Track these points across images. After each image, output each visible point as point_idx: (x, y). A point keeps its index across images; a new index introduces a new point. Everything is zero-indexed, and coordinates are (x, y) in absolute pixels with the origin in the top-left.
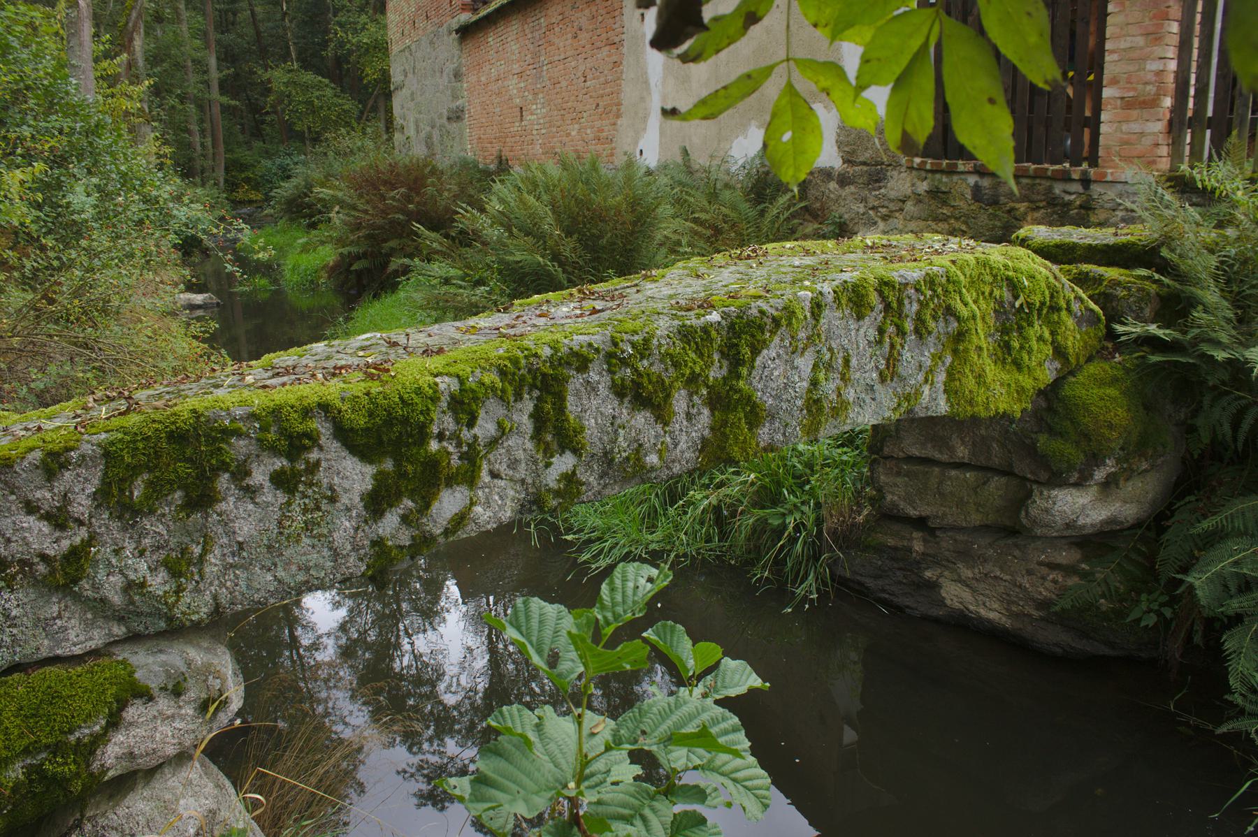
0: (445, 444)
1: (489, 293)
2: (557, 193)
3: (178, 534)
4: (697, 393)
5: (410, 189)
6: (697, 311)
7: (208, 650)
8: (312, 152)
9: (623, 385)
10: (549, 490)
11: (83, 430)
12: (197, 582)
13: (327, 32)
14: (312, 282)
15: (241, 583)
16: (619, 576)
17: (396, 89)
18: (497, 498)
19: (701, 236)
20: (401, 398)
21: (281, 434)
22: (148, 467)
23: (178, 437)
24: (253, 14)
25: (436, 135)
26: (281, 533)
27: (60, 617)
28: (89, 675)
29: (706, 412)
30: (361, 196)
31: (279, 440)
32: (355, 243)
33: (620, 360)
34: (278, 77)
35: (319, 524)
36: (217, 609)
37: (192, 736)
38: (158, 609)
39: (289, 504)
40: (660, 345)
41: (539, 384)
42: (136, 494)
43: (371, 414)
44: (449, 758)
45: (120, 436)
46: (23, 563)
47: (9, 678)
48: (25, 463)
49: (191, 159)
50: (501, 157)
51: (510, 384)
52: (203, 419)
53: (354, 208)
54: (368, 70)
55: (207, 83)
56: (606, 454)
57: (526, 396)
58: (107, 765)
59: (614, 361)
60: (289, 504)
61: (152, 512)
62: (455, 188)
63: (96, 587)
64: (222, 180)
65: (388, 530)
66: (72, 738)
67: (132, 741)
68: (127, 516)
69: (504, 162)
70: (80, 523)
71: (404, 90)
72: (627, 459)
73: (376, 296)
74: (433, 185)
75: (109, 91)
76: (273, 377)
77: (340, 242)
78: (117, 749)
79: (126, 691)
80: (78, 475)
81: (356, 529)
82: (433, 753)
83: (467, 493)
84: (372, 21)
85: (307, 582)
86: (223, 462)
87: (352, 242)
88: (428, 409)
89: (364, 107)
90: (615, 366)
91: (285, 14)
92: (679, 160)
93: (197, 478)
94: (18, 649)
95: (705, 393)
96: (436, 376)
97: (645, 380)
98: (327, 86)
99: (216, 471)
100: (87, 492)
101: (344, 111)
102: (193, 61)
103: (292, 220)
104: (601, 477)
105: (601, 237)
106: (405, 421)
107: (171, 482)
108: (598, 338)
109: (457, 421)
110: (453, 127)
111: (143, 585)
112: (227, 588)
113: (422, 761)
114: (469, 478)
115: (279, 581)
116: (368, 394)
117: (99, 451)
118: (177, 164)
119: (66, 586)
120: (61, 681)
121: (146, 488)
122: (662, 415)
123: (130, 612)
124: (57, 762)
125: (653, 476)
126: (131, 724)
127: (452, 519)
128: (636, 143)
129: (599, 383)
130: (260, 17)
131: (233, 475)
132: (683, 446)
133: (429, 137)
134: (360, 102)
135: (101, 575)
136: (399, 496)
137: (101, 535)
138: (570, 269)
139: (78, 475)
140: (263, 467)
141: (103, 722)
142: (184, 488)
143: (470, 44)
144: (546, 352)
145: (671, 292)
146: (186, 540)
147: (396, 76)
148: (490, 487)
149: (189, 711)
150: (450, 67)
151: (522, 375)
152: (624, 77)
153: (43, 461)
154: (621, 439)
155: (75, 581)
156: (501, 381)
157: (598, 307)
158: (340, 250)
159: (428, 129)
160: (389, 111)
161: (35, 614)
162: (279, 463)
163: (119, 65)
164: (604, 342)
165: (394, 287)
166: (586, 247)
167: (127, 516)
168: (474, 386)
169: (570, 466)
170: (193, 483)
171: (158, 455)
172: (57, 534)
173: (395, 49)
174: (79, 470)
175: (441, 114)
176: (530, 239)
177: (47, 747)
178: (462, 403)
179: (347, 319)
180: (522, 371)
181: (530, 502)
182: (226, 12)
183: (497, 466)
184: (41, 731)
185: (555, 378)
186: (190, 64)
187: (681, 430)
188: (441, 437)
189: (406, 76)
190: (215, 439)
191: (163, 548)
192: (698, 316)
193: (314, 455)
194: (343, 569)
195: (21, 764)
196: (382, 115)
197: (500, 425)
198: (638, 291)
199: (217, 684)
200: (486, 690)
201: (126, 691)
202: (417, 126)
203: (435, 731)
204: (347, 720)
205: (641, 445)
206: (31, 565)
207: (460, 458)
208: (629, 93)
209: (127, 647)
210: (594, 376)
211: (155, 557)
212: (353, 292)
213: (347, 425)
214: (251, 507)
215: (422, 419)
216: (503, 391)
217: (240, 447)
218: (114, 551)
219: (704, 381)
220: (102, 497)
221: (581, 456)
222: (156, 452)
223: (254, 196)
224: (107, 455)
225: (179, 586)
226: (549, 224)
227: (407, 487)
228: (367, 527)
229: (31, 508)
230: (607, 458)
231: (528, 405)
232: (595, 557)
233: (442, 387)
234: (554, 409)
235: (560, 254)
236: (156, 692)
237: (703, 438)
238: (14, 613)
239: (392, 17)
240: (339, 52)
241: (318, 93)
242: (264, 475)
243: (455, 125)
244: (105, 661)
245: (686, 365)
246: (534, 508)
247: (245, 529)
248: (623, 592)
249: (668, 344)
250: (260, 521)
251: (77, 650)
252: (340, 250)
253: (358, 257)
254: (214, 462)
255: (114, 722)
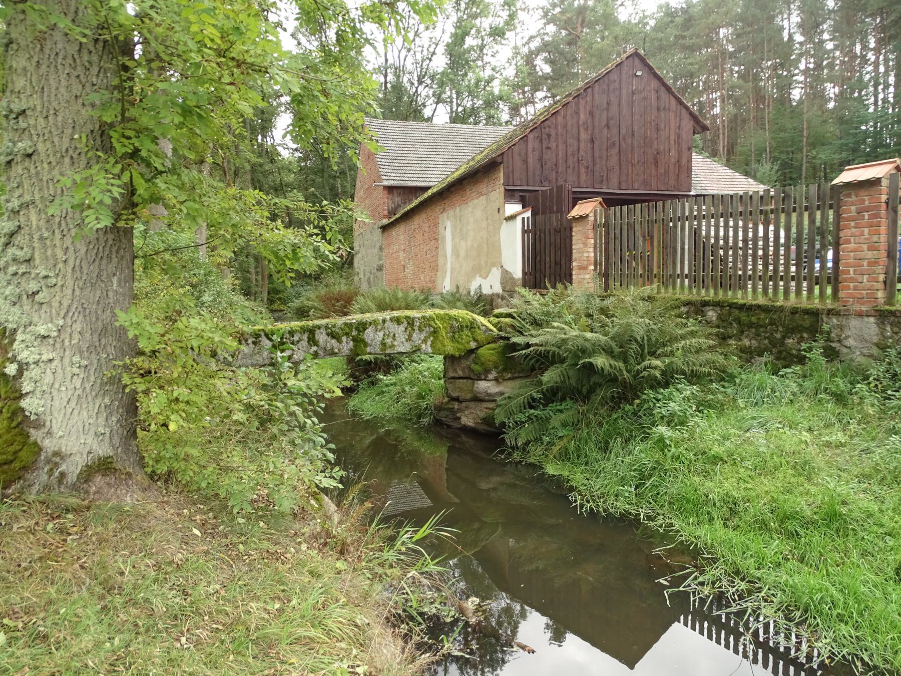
25: (372, 277)
49: (249, 287)
64: (266, 299)
118: (242, 289)
122: (339, 341)
133: (369, 278)
143: (386, 234)
150: (379, 244)
208: (441, 261)
230: (325, 349)
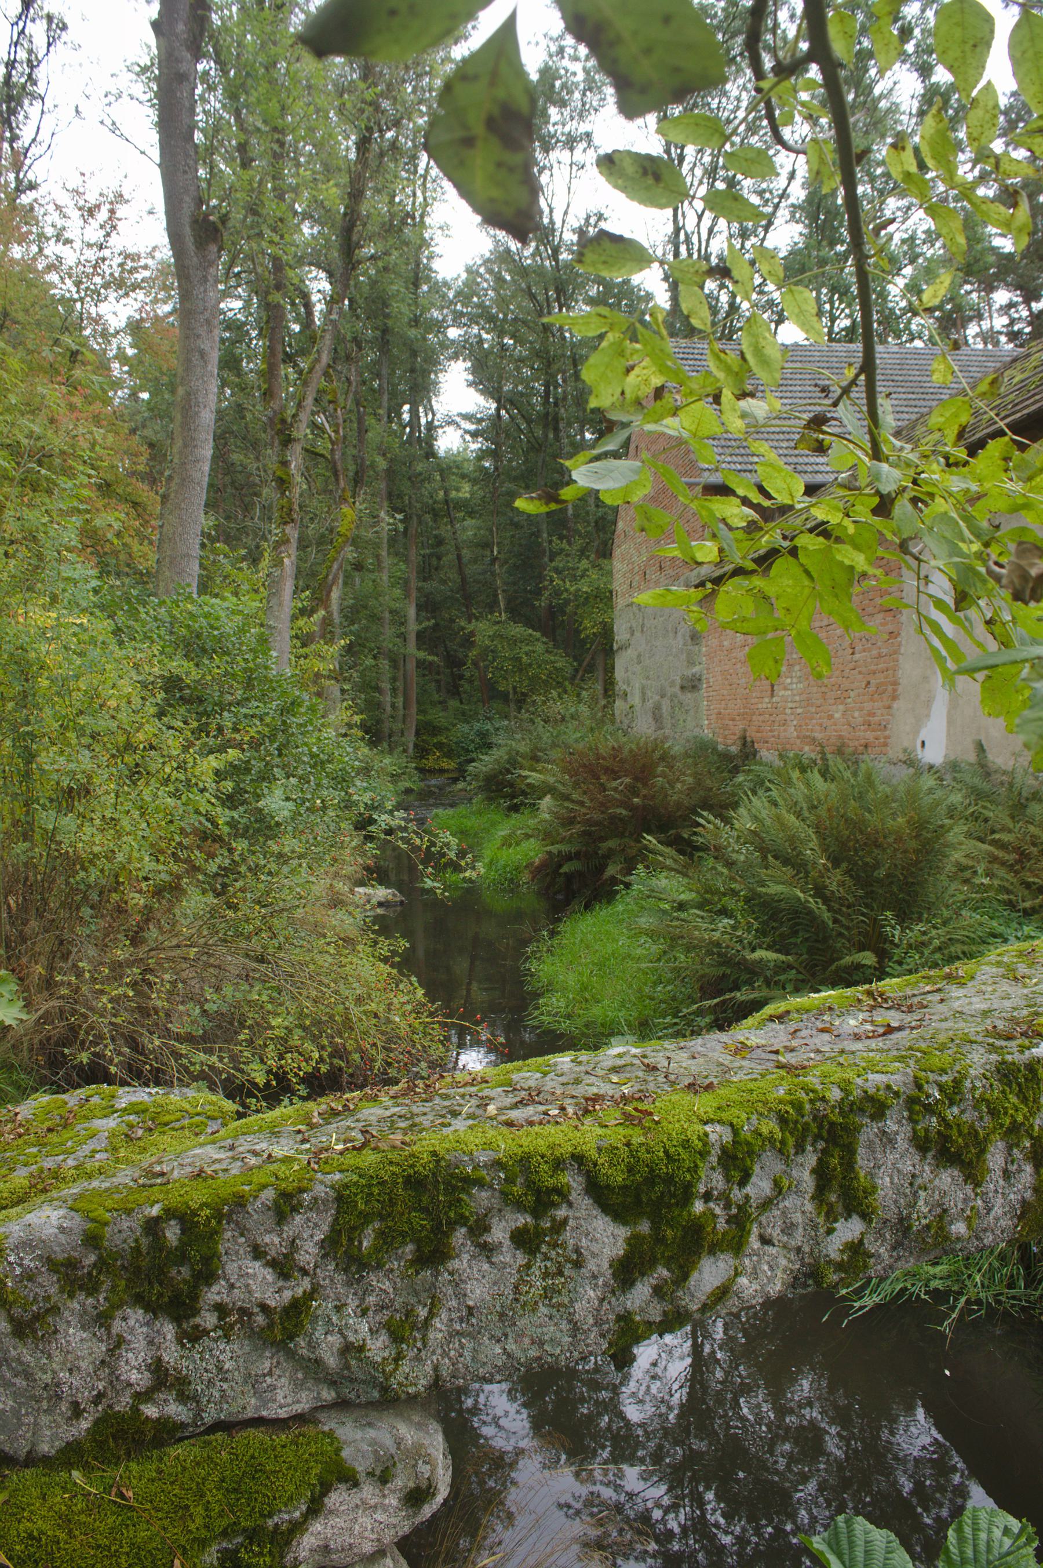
0: (711, 1205)
1: (734, 928)
2: (823, 812)
3: (404, 1293)
4: (1018, 1146)
5: (636, 779)
6: (1019, 1042)
7: (420, 1426)
8: (516, 717)
9: (926, 1137)
10: (829, 1262)
11: (316, 1167)
12: (419, 1350)
13: (541, 578)
14: (511, 881)
15: (466, 1354)
16: (969, 1521)
17: (620, 648)
18: (766, 1268)
19: (1003, 864)
20: (666, 1152)
21: (528, 1186)
22: (380, 1215)
23: (415, 1183)
24: (459, 557)
26: (517, 1300)
27: (270, 1374)
28: (294, 1447)
29: (1029, 1169)
30: (576, 785)
31: (526, 1194)
32: (570, 841)
33: (924, 1106)
34: (483, 629)
35: (559, 1292)
36: (436, 1383)
37: (392, 1532)
38: (375, 1377)
39: (528, 1266)
40: (974, 1088)
41: (825, 1134)
42: (365, 1244)
43: (631, 1170)
44: (627, 1493)
45: (355, 1178)
46: (243, 1311)
47: (212, 1437)
48: (258, 1204)
50: (745, 738)
51: (791, 1133)
52: (443, 1163)
53: (567, 798)
54: (587, 623)
55: (403, 636)
56: (901, 1220)
57: (809, 1148)
58: (300, 1558)
59: (917, 1108)
60: (528, 1266)
61: (379, 1266)
62: (690, 780)
63: (312, 1346)
64: (411, 746)
65: (638, 1302)
66: (270, 1523)
67: (329, 1532)
68: (354, 1269)
69: (749, 744)
70: (305, 1272)
71: (629, 651)
72: (928, 1227)
73: (588, 907)
74: (664, 775)
75: (302, 651)
76: (515, 1106)
77: (548, 836)
78: (313, 1540)
79: (332, 1472)
80: (308, 1220)
81: (602, 1300)
82: (607, 1485)
83: (732, 1262)
84: (593, 567)
85: (540, 1358)
86: (462, 1216)
87: (564, 839)
88: (696, 1166)
89: (580, 665)
90: (918, 1113)
91: (496, 559)
92: (972, 757)
93: (432, 1231)
94: (225, 1406)
95: (1028, 1145)
96: (706, 1123)
97: (954, 1132)
98: (538, 640)
99: (452, 1225)
100: (316, 1238)
101: (556, 669)
102: (391, 612)
103: (490, 799)
104: (894, 1248)
105: (877, 866)
106: (669, 1179)
107: (403, 1234)
108: (899, 1077)
109: (728, 1179)
110: (688, 697)
111: (361, 1349)
112: (450, 1358)
113: (592, 1493)
114: (736, 1245)
115: (509, 1355)
116: (628, 1144)
117: (332, 1194)
119: (283, 1341)
120: (265, 1451)
121: (375, 1238)
123: (344, 1377)
124: (252, 1550)
125: (958, 1247)
126: (331, 1512)
127: (712, 1294)
128: (917, 732)
129: (897, 1133)
130: (465, 560)
131: (471, 1230)
132: (997, 1211)
133: (657, 707)
134: (575, 659)
135: (319, 1333)
136: (653, 1263)
137: (325, 1287)
138: (836, 906)
139: (308, 1220)
140: (504, 1223)
141: (304, 1508)
142: (418, 1241)
144: (835, 1094)
145: (984, 1006)
146: (413, 1300)
147: (621, 633)
148: (758, 1255)
149: (393, 1501)
151: (806, 1123)
152: (902, 651)
153: (275, 1202)
154: (921, 1203)
155: (291, 1338)
156: (781, 1130)
157: (895, 1024)
158: (549, 848)
159: (657, 698)
160: (610, 670)
161: (246, 1368)
162: (523, 1220)
163: (315, 624)
164: (905, 1084)
165: (610, 897)
166: (857, 879)
167: (354, 1269)
168: (749, 1137)
169: (857, 1234)
170: (426, 1237)
171: (392, 1203)
172: (280, 1283)
173: (620, 602)
174: (309, 1214)
175: (673, 681)
176: (789, 871)
177: (245, 1530)
178: (735, 1158)
179: (553, 934)
180: (806, 1118)
181: (805, 1275)
182: (431, 555)
183: (769, 1230)
184: (241, 1510)
185: (845, 1128)
186: (387, 615)
187: (996, 1191)
188: (707, 1197)
189: (632, 635)
190: (455, 1188)
191: (387, 1308)
192: (1022, 1049)
193: (561, 1213)
194: (582, 1347)
195: (217, 1547)
196: (600, 674)
197: (777, 1184)
198: (942, 1000)
199: (425, 1469)
200: (682, 1406)
201: (332, 1472)
202: (643, 694)
203: (611, 1453)
204: (502, 1422)
205: (945, 1211)
206: (250, 1315)
207: (727, 1222)
209: (333, 1414)
210: (891, 1125)
211: (377, 1318)
212: (560, 897)
213: (602, 1181)
214: (486, 1266)
215: (688, 1177)
216: (783, 1142)
217: (482, 1199)
218: (336, 1307)
219: (1027, 1131)
220: (330, 1245)
221: (871, 1221)
222: (390, 1200)
223: (446, 764)
224: (339, 1198)
225: (399, 1353)
226: (812, 851)
227: (663, 1253)
228: (613, 1299)
229: (258, 1252)
230: (903, 1225)
231: (811, 1159)
232: (859, 1293)
233: (713, 1137)
234: (841, 1164)
235: (825, 887)
236: (362, 1477)
237: (1024, 1202)
238: (226, 1367)
239: (619, 565)
240: (554, 602)
241: (527, 648)
242: (504, 1232)
243: (689, 695)
244: (309, 1430)
245: (1006, 1113)
246: (810, 1282)
247: (477, 1292)
248: (975, 1546)
249: (984, 1086)
250: (495, 1283)
251: (283, 1413)
252: (549, 848)
253: (569, 857)
254: (452, 1215)
255: (315, 1509)
